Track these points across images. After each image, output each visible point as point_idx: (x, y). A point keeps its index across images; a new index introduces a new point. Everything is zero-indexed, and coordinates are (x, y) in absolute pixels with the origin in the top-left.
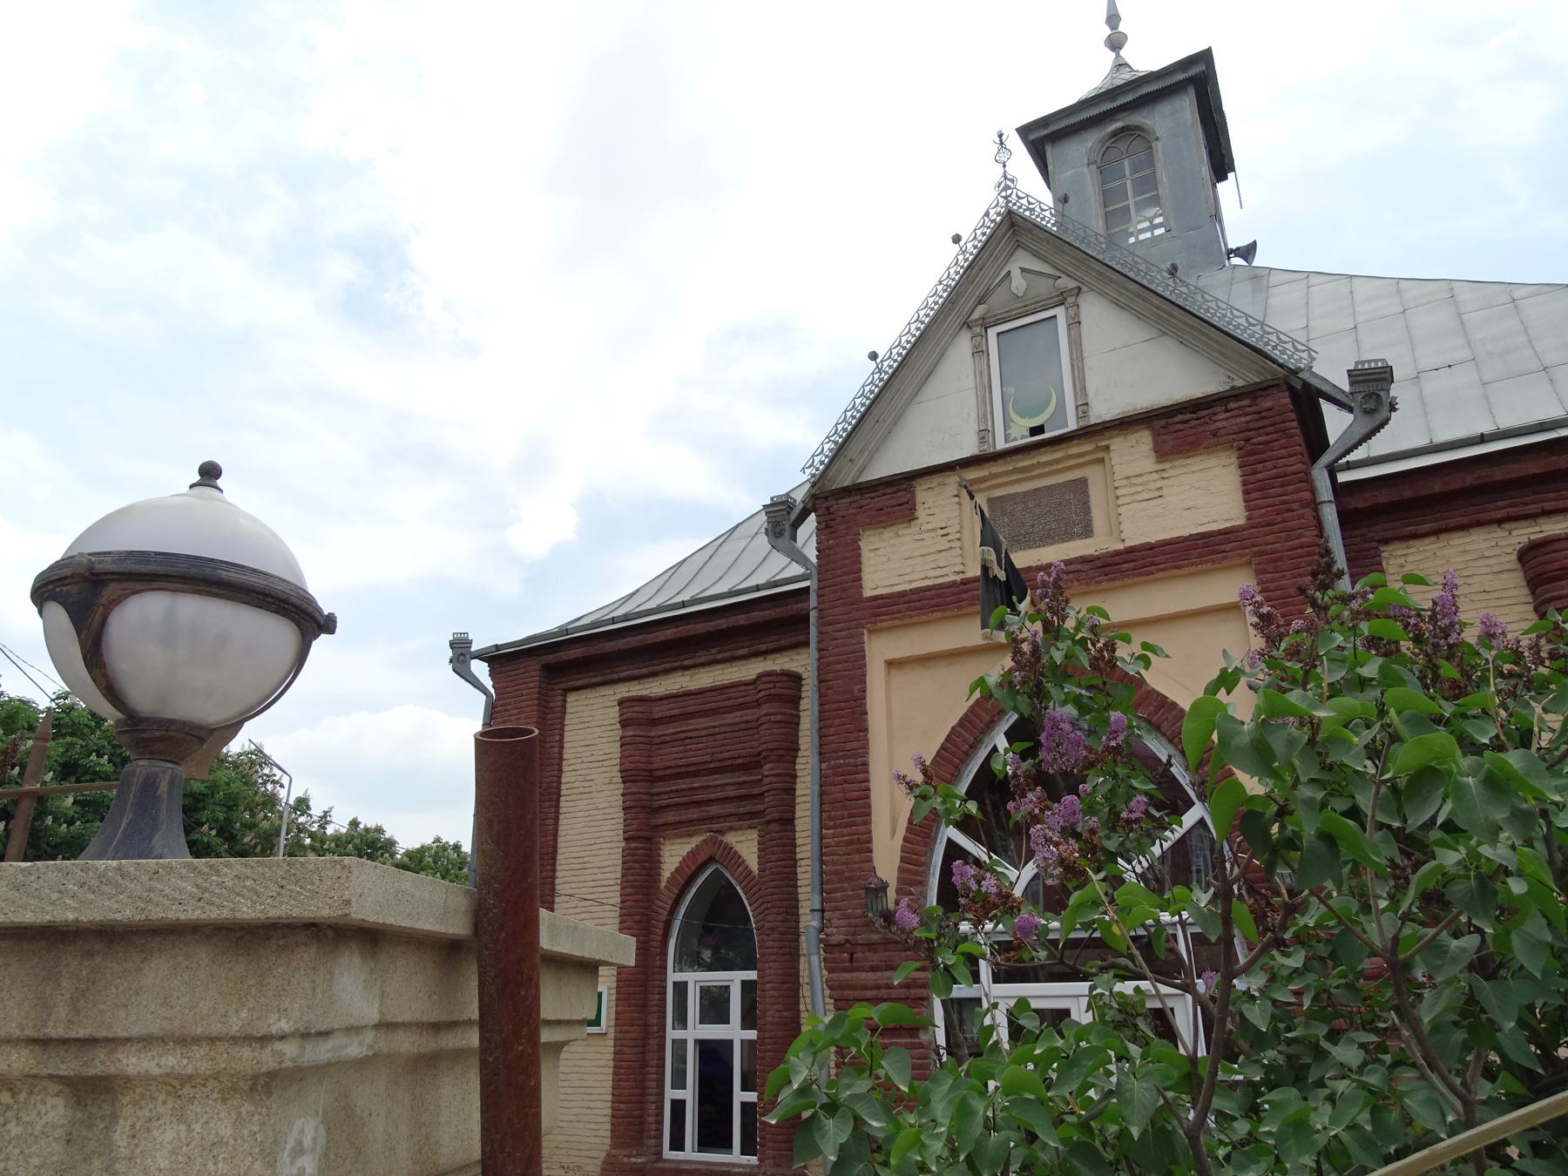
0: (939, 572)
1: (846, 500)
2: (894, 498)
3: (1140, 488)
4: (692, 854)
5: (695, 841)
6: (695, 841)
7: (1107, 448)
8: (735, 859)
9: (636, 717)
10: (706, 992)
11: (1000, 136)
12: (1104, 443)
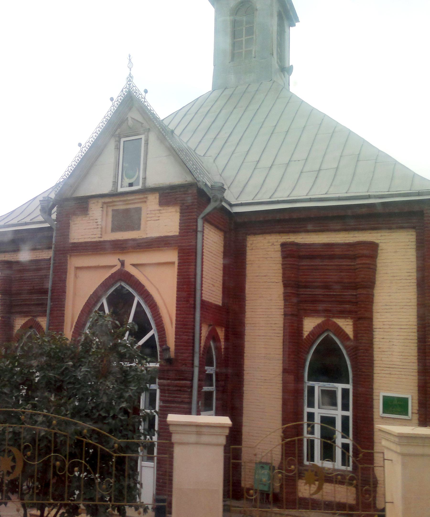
0: (93, 236)
1: (69, 203)
2: (82, 204)
3: (154, 215)
4: (319, 326)
5: (27, 319)
6: (27, 319)
7: (146, 198)
8: (39, 327)
9: (290, 253)
10: (324, 392)
11: (130, 56)
12: (145, 196)
